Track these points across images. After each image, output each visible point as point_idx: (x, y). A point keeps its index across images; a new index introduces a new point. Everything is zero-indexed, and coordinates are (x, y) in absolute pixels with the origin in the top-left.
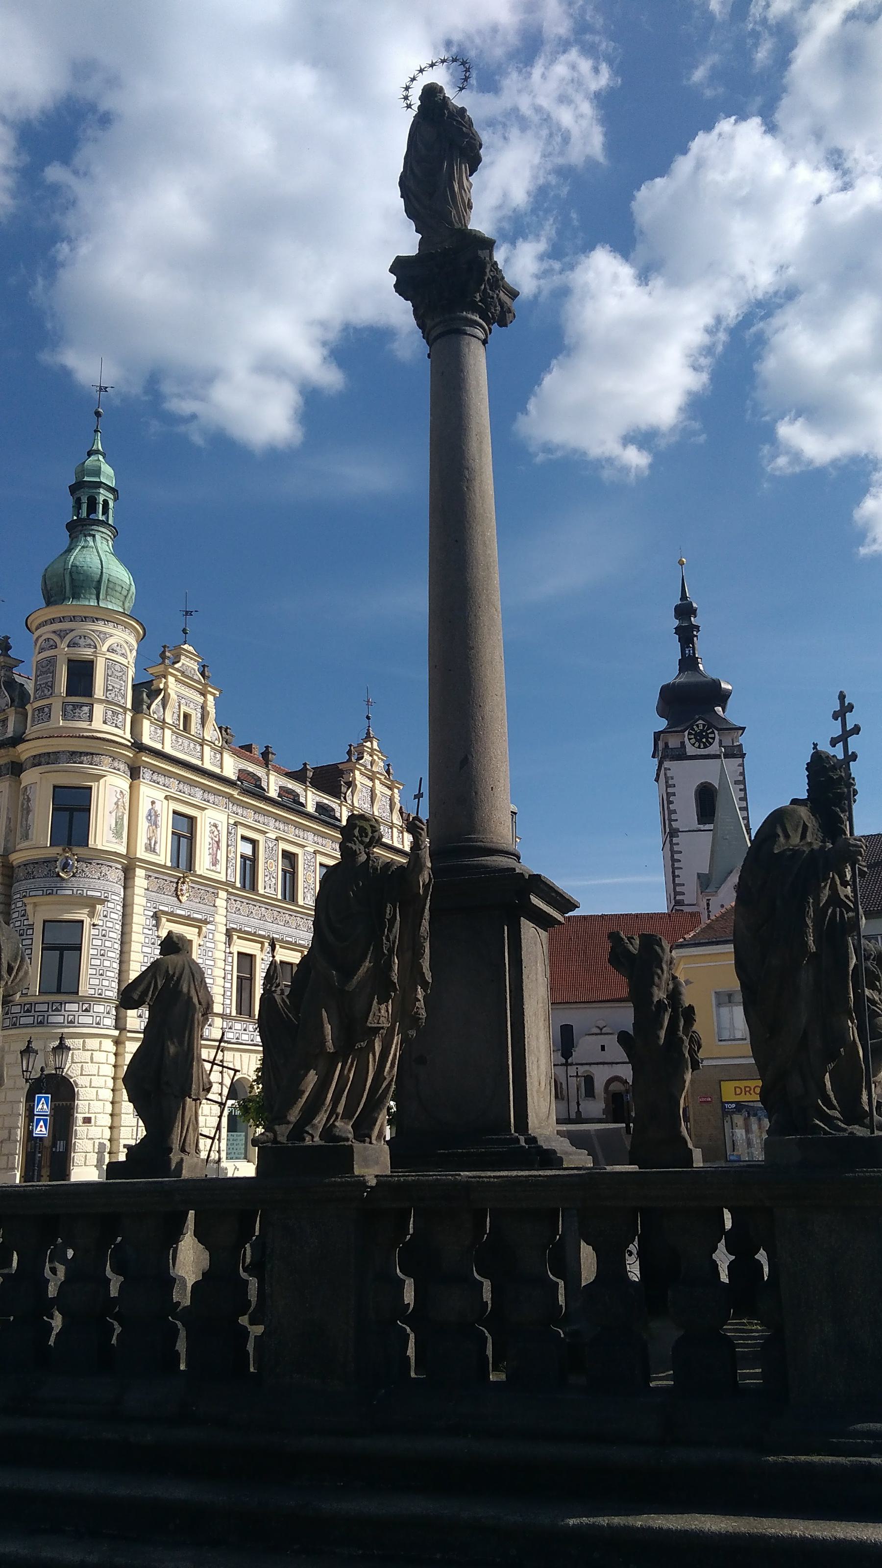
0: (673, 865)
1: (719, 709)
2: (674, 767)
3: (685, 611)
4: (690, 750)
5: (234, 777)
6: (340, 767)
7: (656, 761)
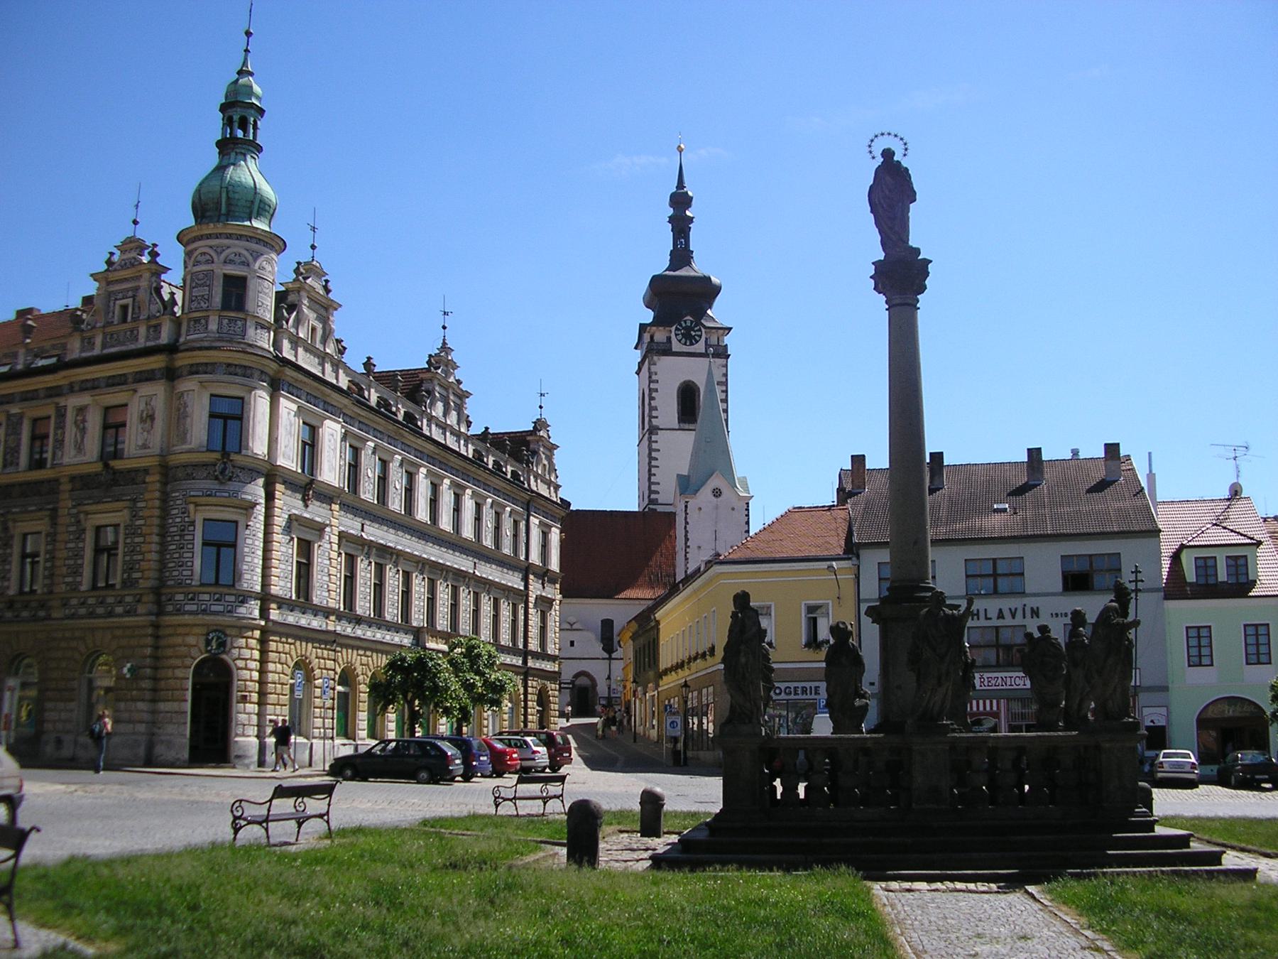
3: (680, 201)
4: (676, 346)
7: (638, 355)
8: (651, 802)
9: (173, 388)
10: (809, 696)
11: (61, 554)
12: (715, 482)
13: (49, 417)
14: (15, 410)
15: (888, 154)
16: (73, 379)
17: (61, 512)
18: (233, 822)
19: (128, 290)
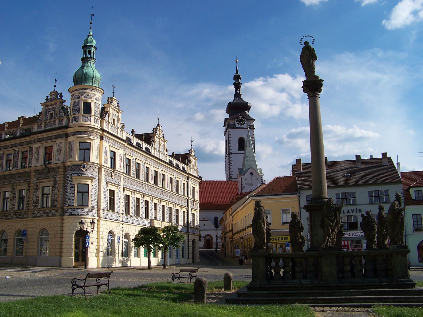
0: (229, 165)
1: (246, 112)
2: (232, 131)
4: (237, 126)
5: (125, 139)
6: (151, 135)
7: (224, 129)
8: (227, 279)
9: (67, 140)
10: (283, 241)
11: (32, 196)
12: (250, 171)
13: (27, 151)
14: (16, 149)
15: (306, 43)
16: (35, 138)
17: (31, 182)
18: (72, 287)
19: (52, 108)
